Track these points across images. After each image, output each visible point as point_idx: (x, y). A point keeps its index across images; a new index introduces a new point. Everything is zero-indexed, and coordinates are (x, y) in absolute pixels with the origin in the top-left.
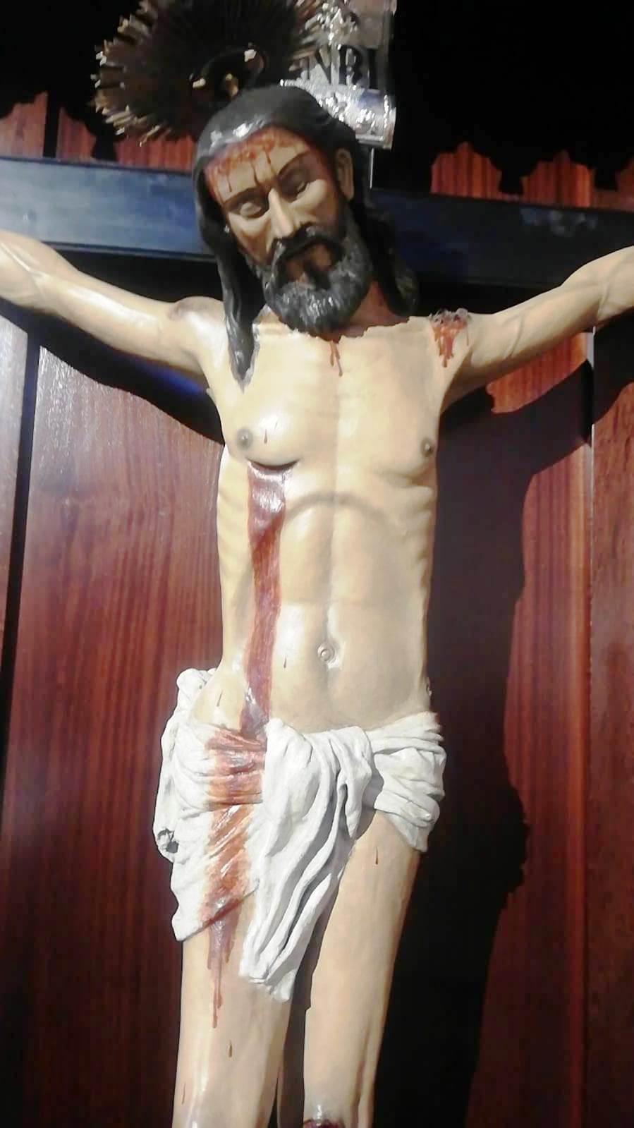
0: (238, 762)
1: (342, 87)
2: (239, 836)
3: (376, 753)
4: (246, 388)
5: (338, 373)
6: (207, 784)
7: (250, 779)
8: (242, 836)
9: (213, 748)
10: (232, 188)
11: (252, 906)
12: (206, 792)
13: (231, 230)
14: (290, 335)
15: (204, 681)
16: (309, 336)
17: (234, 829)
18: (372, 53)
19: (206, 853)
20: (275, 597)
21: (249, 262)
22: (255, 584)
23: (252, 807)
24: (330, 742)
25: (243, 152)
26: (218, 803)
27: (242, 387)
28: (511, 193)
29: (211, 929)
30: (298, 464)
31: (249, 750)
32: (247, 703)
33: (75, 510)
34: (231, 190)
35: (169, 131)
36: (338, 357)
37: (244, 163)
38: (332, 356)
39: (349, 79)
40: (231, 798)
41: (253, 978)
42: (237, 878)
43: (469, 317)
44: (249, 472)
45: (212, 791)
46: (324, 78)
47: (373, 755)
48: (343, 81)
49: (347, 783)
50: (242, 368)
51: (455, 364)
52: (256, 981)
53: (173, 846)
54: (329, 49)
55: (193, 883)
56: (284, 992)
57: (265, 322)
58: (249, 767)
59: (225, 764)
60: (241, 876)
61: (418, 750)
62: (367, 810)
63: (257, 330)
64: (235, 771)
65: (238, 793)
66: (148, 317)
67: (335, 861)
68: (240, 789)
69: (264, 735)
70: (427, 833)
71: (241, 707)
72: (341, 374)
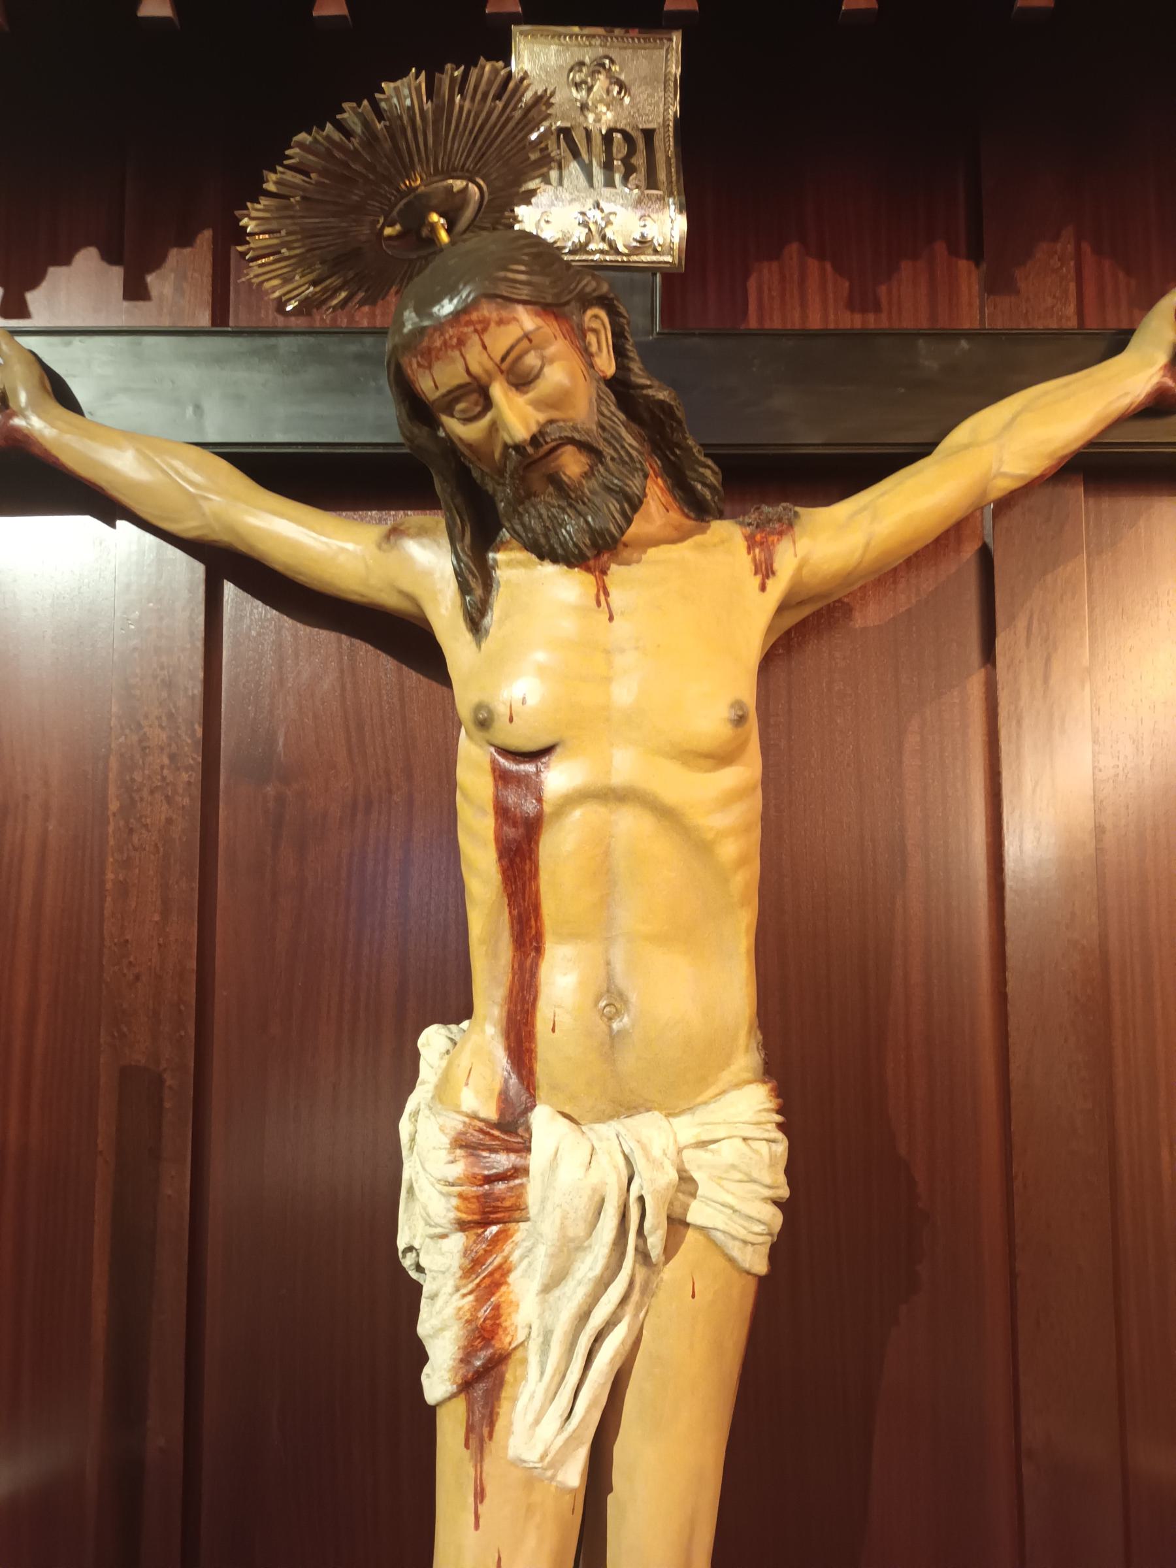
0: (494, 1168)
1: (607, 191)
2: (500, 1267)
3: (685, 1147)
4: (483, 645)
5: (607, 616)
6: (455, 1196)
7: (511, 1189)
8: (504, 1266)
9: (461, 1147)
10: (438, 385)
11: (524, 1361)
12: (453, 1206)
13: (447, 434)
14: (540, 567)
15: (451, 1039)
16: (565, 567)
17: (495, 1256)
18: (649, 134)
19: (457, 1290)
20: (536, 933)
21: (475, 474)
22: (510, 913)
23: (516, 1228)
24: (618, 1137)
25: (447, 336)
26: (469, 1222)
27: (479, 643)
28: (864, 310)
29: (468, 1393)
30: (559, 750)
31: (509, 1150)
32: (506, 1081)
33: (280, 799)
34: (436, 387)
35: (361, 295)
36: (607, 594)
37: (450, 352)
38: (598, 596)
39: (618, 177)
40: (486, 1216)
41: (525, 1462)
42: (499, 1325)
43: (796, 514)
44: (494, 762)
45: (462, 1208)
46: (582, 180)
47: (680, 1151)
48: (610, 183)
49: (643, 1193)
50: (475, 620)
51: (778, 588)
52: (531, 1465)
53: (419, 1269)
54: (588, 133)
55: (442, 1329)
56: (573, 1474)
57: (506, 549)
58: (509, 1173)
59: (476, 1170)
60: (506, 1321)
61: (745, 1139)
62: (677, 1224)
63: (495, 560)
64: (489, 1180)
65: (496, 1210)
66: (350, 546)
67: (635, 1296)
68: (499, 1204)
69: (528, 1130)
70: (765, 1250)
71: (497, 1086)
72: (611, 618)
